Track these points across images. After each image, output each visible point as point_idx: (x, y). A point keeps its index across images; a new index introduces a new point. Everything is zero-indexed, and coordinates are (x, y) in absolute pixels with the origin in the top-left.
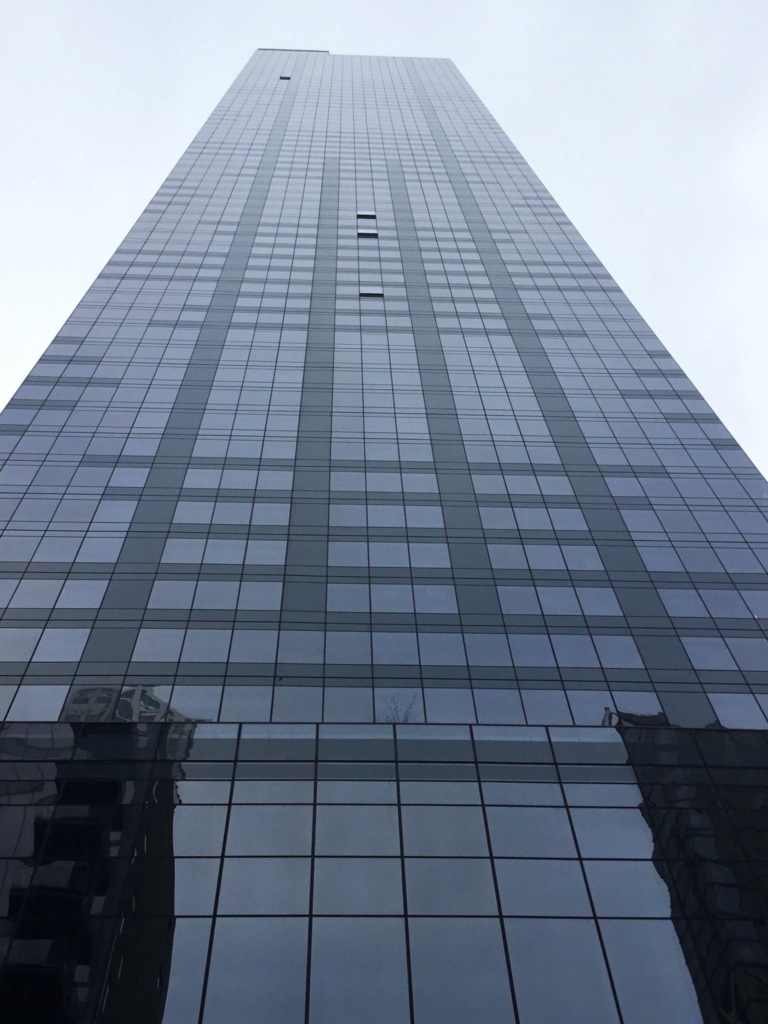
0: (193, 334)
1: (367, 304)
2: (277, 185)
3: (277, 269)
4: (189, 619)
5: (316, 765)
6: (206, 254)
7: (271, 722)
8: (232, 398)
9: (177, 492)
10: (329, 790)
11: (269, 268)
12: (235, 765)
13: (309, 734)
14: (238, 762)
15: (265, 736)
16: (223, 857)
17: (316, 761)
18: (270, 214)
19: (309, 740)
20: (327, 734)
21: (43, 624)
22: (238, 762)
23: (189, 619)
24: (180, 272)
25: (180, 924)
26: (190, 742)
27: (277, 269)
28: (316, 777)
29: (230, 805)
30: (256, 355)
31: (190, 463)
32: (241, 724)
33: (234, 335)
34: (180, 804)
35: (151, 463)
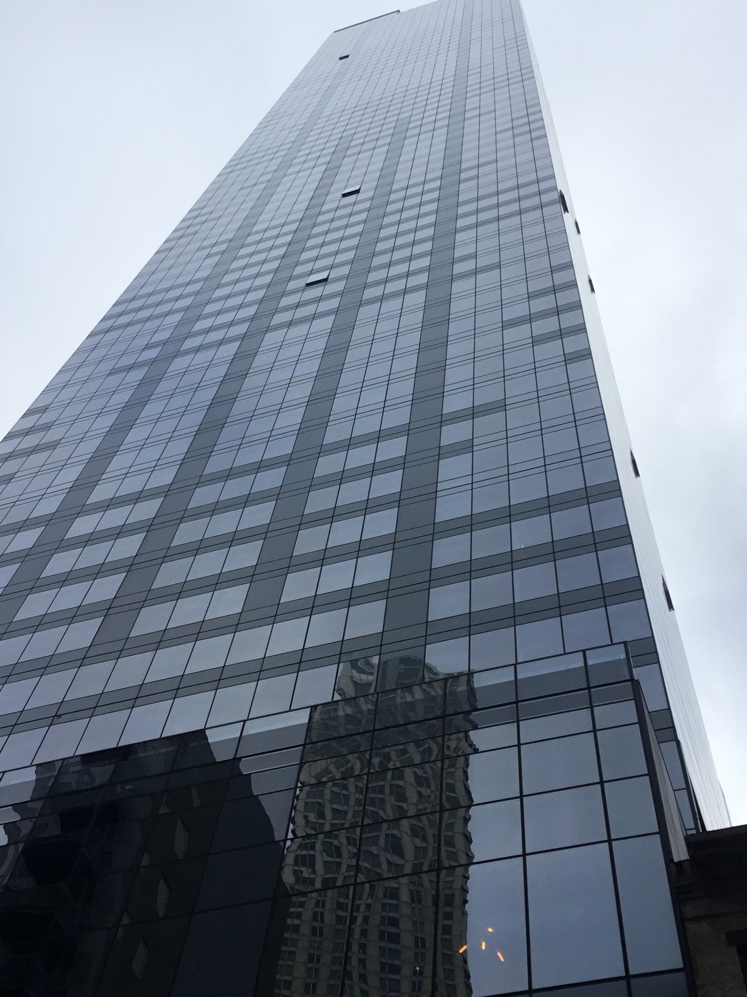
0: (420, 297)
1: (316, 292)
2: (471, 127)
3: (506, 203)
4: (470, 571)
5: (590, 693)
6: (498, 193)
7: (565, 654)
8: (466, 347)
9: (436, 451)
10: (531, 729)
11: (519, 199)
12: (590, 693)
13: (507, 676)
14: (520, 703)
15: (610, 659)
16: (521, 797)
17: (589, 688)
18: (469, 158)
19: (575, 669)
20: (524, 673)
21: (233, 629)
22: (520, 703)
23: (470, 571)
24: (482, 217)
25: (734, 825)
26: (471, 690)
27: (506, 203)
28: (591, 704)
29: (519, 745)
30: (482, 300)
31: (443, 420)
32: (584, 651)
33: (458, 287)
34: (476, 751)
35: (407, 430)
